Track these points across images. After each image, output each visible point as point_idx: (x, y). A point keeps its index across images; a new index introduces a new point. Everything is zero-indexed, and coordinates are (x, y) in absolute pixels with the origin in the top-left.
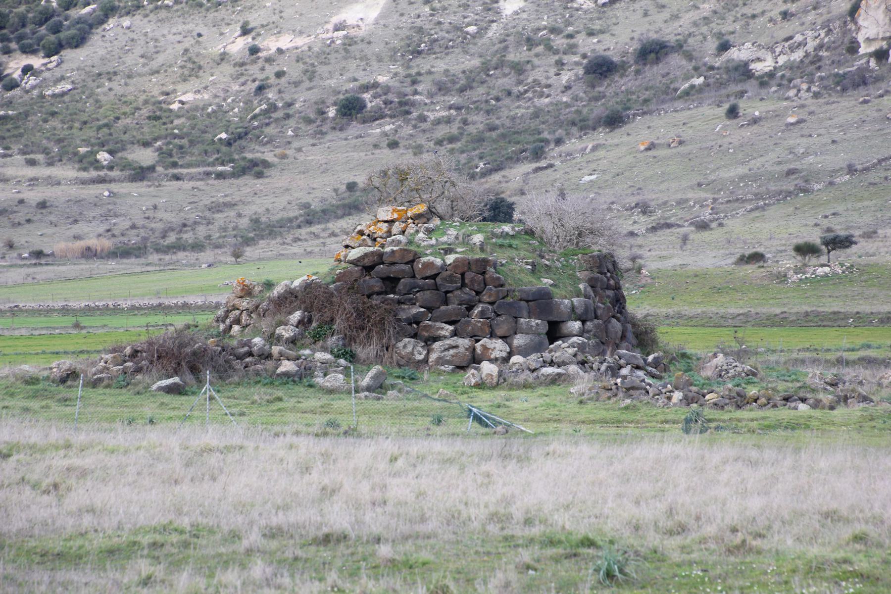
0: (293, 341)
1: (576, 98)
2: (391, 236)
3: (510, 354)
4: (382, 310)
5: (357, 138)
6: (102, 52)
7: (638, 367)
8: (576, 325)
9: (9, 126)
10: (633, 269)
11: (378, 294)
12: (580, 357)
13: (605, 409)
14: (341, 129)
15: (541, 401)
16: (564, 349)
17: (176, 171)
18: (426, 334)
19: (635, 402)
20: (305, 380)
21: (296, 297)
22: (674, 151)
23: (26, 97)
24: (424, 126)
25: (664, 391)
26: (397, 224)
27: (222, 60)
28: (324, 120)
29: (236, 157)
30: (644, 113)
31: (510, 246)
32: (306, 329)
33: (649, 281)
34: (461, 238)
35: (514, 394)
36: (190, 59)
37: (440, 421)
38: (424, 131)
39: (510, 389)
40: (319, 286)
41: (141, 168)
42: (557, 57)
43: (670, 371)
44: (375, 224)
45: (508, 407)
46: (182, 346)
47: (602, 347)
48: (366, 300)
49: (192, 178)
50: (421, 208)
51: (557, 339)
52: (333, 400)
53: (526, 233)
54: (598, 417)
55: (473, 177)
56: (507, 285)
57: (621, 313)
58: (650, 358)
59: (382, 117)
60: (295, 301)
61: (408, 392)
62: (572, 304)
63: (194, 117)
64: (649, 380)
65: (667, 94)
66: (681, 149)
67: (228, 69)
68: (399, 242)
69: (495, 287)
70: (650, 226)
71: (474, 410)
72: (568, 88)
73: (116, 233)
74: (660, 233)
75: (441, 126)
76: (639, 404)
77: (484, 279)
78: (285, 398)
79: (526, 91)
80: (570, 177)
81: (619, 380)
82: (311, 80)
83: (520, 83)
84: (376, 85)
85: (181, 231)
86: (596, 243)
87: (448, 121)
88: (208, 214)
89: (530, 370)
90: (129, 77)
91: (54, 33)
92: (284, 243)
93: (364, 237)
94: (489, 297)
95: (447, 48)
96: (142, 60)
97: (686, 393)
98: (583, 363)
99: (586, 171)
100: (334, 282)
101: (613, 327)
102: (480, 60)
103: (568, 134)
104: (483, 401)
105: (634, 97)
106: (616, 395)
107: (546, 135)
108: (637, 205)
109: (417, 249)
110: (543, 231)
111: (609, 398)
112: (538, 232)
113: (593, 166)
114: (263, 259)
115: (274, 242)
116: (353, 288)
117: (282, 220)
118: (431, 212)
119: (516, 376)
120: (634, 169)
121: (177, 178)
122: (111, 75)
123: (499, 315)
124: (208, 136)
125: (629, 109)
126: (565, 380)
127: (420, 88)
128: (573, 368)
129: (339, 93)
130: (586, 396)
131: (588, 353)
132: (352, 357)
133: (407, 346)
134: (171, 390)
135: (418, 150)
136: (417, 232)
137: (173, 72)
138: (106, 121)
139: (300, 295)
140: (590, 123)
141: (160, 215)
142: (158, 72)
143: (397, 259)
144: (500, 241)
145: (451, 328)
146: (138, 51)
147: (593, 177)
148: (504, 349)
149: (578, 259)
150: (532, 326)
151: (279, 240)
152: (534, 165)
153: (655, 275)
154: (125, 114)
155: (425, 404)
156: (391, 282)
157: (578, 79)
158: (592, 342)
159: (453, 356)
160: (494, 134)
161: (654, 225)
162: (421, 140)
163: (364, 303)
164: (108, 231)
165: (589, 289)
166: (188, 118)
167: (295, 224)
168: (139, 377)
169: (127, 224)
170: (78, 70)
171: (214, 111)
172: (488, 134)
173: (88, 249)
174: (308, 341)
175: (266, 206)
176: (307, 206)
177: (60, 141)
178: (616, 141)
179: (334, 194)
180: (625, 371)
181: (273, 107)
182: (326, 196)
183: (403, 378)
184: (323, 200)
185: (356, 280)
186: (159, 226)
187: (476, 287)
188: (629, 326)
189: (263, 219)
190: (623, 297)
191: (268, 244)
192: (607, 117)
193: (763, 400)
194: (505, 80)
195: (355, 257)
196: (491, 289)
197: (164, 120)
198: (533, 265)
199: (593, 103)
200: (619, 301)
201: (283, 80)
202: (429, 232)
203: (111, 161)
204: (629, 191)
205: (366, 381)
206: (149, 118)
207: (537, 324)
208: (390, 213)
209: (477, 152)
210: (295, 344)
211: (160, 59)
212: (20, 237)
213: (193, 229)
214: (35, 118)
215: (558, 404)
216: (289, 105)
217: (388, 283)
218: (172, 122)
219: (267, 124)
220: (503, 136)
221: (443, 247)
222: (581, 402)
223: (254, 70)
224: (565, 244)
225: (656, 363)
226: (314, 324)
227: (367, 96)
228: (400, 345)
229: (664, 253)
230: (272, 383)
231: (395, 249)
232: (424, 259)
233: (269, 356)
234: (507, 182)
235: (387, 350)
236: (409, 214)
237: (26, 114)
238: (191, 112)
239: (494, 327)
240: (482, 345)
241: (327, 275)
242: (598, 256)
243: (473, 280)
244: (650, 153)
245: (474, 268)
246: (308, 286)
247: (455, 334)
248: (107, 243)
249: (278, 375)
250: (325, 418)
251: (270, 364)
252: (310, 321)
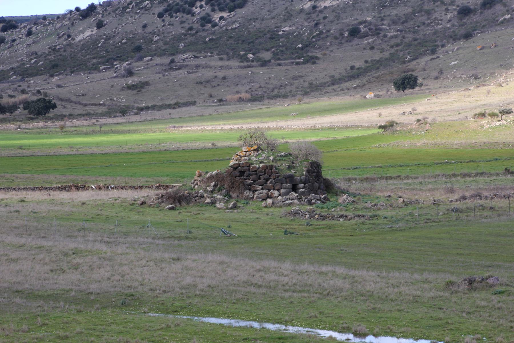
0: (212, 192)
1: (453, 25)
5: (357, 45)
6: (252, 10)
7: (318, 200)
8: (302, 185)
9: (213, 43)
11: (238, 176)
14: (350, 42)
17: (279, 62)
22: (492, 50)
23: (221, 30)
24: (385, 39)
27: (301, 12)
28: (343, 37)
29: (305, 55)
30: (482, 32)
36: (288, 12)
38: (386, 42)
41: (265, 61)
42: (446, 7)
46: (176, 194)
49: (286, 65)
55: (404, 62)
59: (368, 36)
63: (289, 38)
65: (494, 23)
66: (496, 49)
67: (303, 16)
72: (450, 21)
73: (253, 90)
75: (393, 40)
79: (431, 23)
82: (338, 20)
83: (429, 19)
84: (365, 22)
85: (280, 89)
87: (396, 37)
88: (291, 81)
90: (263, 20)
91: (233, 2)
92: (321, 94)
95: (397, 4)
96: (268, 13)
102: (412, 9)
103: (448, 42)
105: (479, 24)
107: (438, 43)
121: (280, 65)
122: (255, 20)
124: (294, 46)
125: (475, 30)
127: (385, 22)
129: (350, 25)
133: (247, 193)
134: (170, 209)
135: (382, 51)
137: (281, 18)
138: (252, 40)
140: (458, 37)
141: (272, 81)
142: (274, 18)
143: (244, 165)
145: (261, 187)
146: (267, 9)
147: (456, 62)
151: (319, 92)
154: (260, 37)
156: (242, 173)
157: (454, 16)
160: (416, 42)
162: (384, 46)
164: (250, 89)
166: (286, 38)
167: (327, 85)
168: (163, 204)
169: (258, 86)
170: (242, 17)
171: (297, 35)
172: (413, 43)
173: (240, 98)
174: (216, 191)
176: (333, 77)
177: (233, 49)
178: (468, 45)
181: (321, 33)
184: (340, 74)
186: (271, 86)
189: (314, 83)
192: (465, 34)
193: (330, 218)
194: (423, 18)
197: (276, 39)
199: (461, 28)
201: (326, 20)
203: (253, 58)
205: (231, 205)
206: (270, 38)
211: (276, 12)
212: (214, 92)
213: (285, 88)
214: (223, 39)
216: (328, 31)
218: (279, 40)
219: (319, 40)
220: (419, 43)
223: (314, 16)
226: (219, 186)
227: (361, 27)
228: (245, 192)
229: (478, 99)
233: (203, 197)
236: (252, 149)
237: (220, 37)
238: (287, 35)
244: (482, 51)
246: (217, 174)
247: (262, 189)
248: (248, 96)
251: (203, 199)
252: (217, 185)
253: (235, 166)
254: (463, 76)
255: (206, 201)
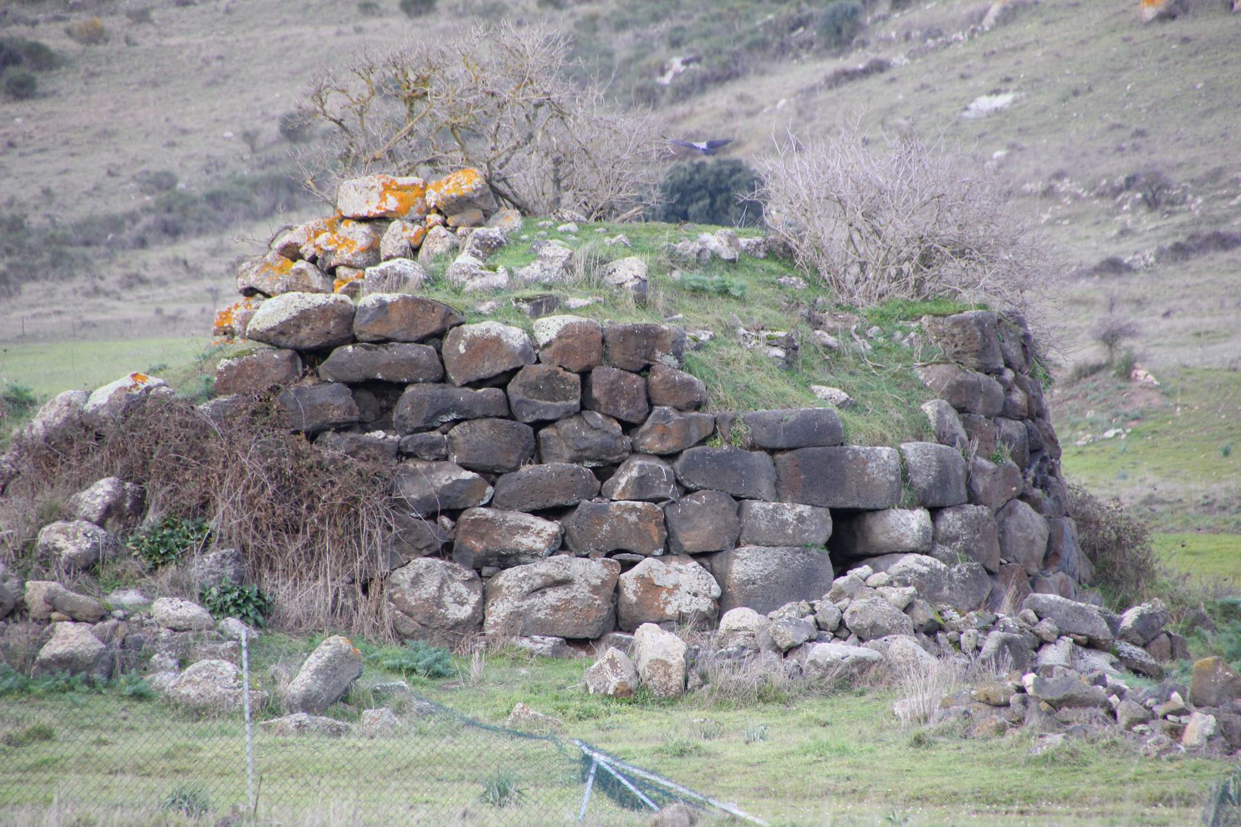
2: (377, 261)
3: (722, 604)
4: (349, 477)
7: (1091, 644)
8: (914, 521)
10: (1107, 366)
11: (341, 428)
12: (924, 613)
13: (989, 763)
15: (805, 739)
16: (874, 591)
18: (478, 546)
19: (1074, 742)
20: (123, 679)
21: (99, 437)
25: (1160, 710)
26: (396, 225)
31: (724, 292)
32: (128, 530)
33: (1157, 400)
34: (580, 270)
35: (731, 717)
37: (504, 792)
39: (720, 704)
40: (169, 406)
43: (1186, 656)
44: (332, 227)
45: (708, 755)
47: (989, 584)
48: (304, 446)
50: (467, 182)
51: (857, 560)
52: (201, 735)
53: (771, 254)
54: (968, 784)
56: (712, 405)
57: (1044, 486)
58: (1129, 618)
60: (97, 450)
61: (422, 714)
62: (903, 461)
64: (1116, 678)
68: (402, 279)
69: (680, 410)
70: (1169, 243)
71: (599, 758)
74: (1198, 262)
76: (1085, 748)
77: (647, 388)
78: (60, 732)
80: (934, 98)
81: (1029, 679)
86: (974, 283)
89: (778, 649)
92: (97, 291)
93: (301, 264)
94: (662, 439)
97: (1225, 717)
98: (931, 631)
99: (982, 82)
100: (210, 395)
101: (1020, 528)
104: (636, 739)
106: (1019, 722)
108: (1131, 182)
109: (451, 300)
110: (819, 250)
111: (1001, 730)
112: (804, 251)
113: (1003, 66)
114: (34, 338)
115: (65, 287)
116: (267, 411)
117: (89, 222)
118: (498, 194)
119: (733, 668)
120: (1125, 76)
123: (688, 491)
126: (879, 680)
128: (903, 645)
130: (933, 725)
131: (948, 600)
132: (261, 611)
133: (425, 580)
136: (455, 249)
139: (110, 431)
143: (393, 327)
144: (694, 277)
145: (551, 527)
148: (703, 589)
149: (921, 331)
150: (785, 523)
151: (81, 281)
152: (831, 65)
153: (1174, 383)
155: (470, 745)
156: (378, 393)
158: (961, 569)
159: (556, 609)
161: (1181, 239)
163: (298, 455)
165: (951, 416)
167: (128, 235)
174: (134, 565)
175: (43, 182)
176: (163, 182)
179: (244, 148)
180: (1053, 655)
182: (219, 153)
183: (412, 671)
184: (212, 164)
185: (274, 390)
187: (624, 412)
188: (1070, 525)
189: (35, 220)
190: (1053, 440)
191: (50, 293)
195: (274, 322)
196: (666, 416)
198: (791, 347)
200: (1039, 452)
202: (490, 249)
204: (1110, 141)
205: (302, 678)
207: (801, 519)
208: (374, 195)
209: (664, 26)
210: (95, 575)
215: (853, 746)
217: (366, 396)
221: (528, 293)
222: (919, 741)
224: (884, 286)
225: (1146, 633)
226: (153, 517)
228: (403, 576)
229: (1210, 322)
230: (23, 689)
231: (388, 298)
232: (473, 329)
234: (750, 114)
235: (365, 590)
236: (432, 198)
239: (674, 523)
240: (641, 578)
241: (188, 376)
242: (979, 322)
243: (613, 391)
244: (1172, 28)
245: (616, 353)
246: (134, 407)
247: (562, 545)
249: (44, 665)
250: (168, 787)
252: (140, 507)
253: (308, 337)
254: (1064, 186)
255: (53, 648)
